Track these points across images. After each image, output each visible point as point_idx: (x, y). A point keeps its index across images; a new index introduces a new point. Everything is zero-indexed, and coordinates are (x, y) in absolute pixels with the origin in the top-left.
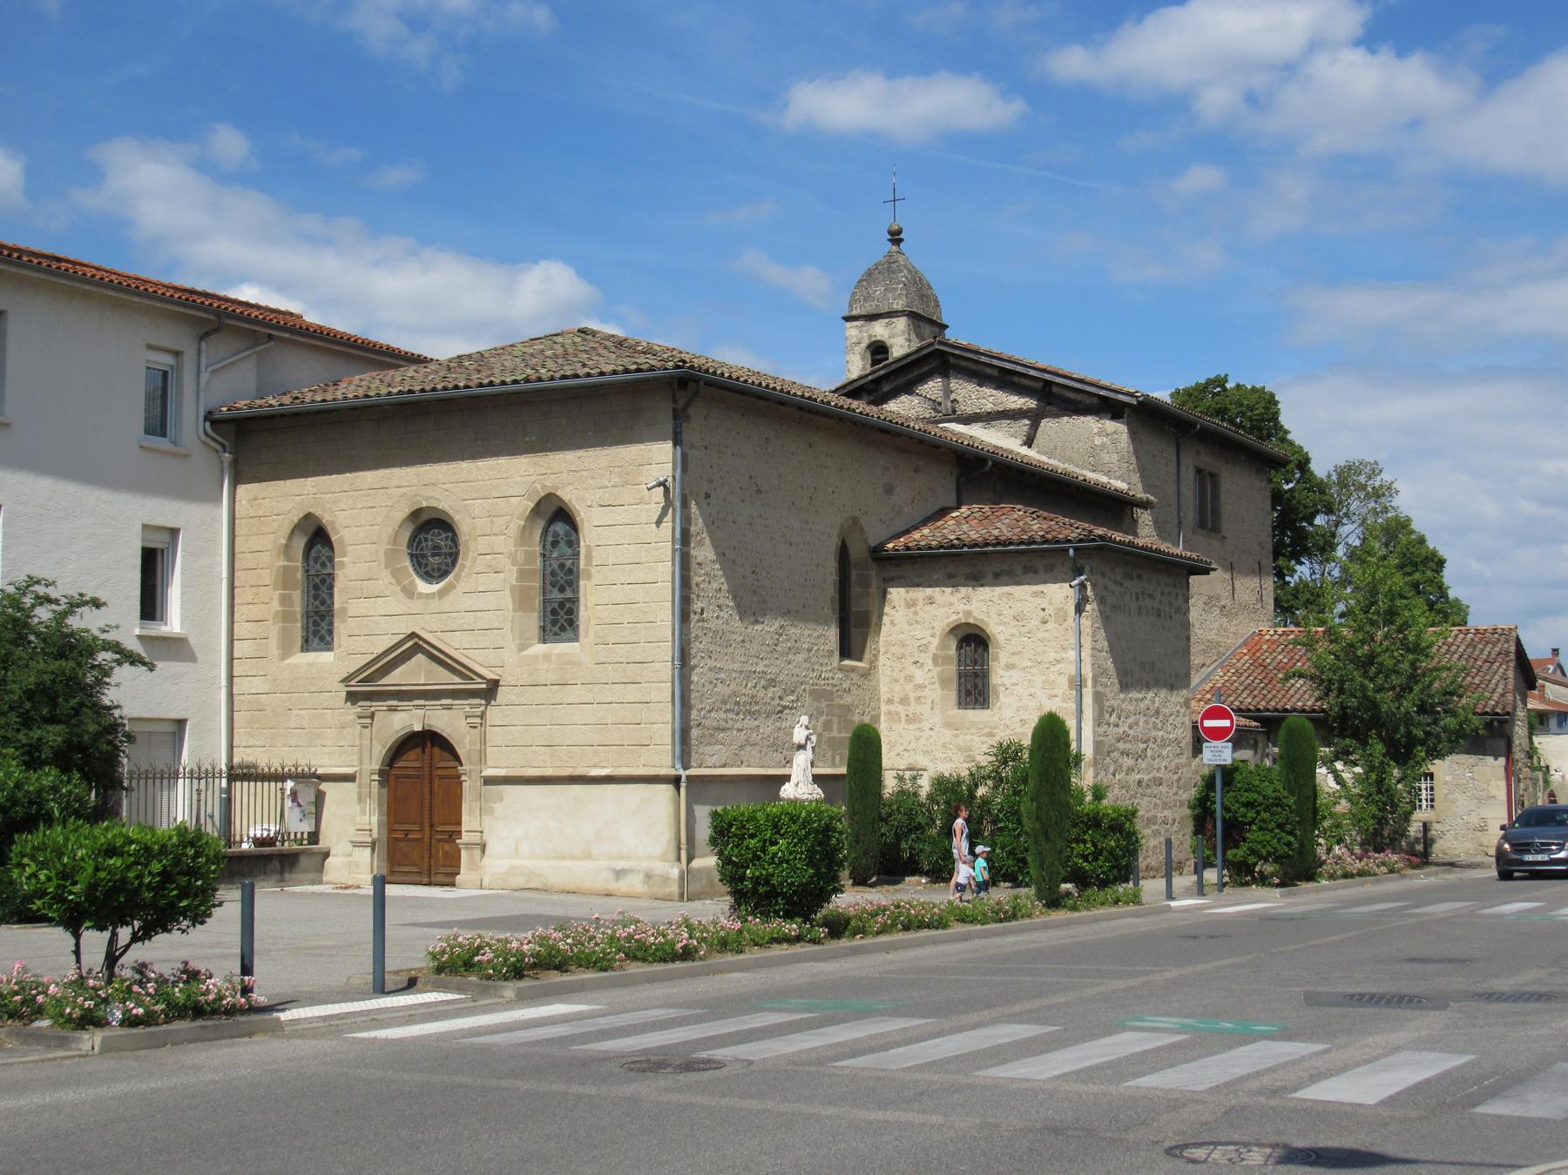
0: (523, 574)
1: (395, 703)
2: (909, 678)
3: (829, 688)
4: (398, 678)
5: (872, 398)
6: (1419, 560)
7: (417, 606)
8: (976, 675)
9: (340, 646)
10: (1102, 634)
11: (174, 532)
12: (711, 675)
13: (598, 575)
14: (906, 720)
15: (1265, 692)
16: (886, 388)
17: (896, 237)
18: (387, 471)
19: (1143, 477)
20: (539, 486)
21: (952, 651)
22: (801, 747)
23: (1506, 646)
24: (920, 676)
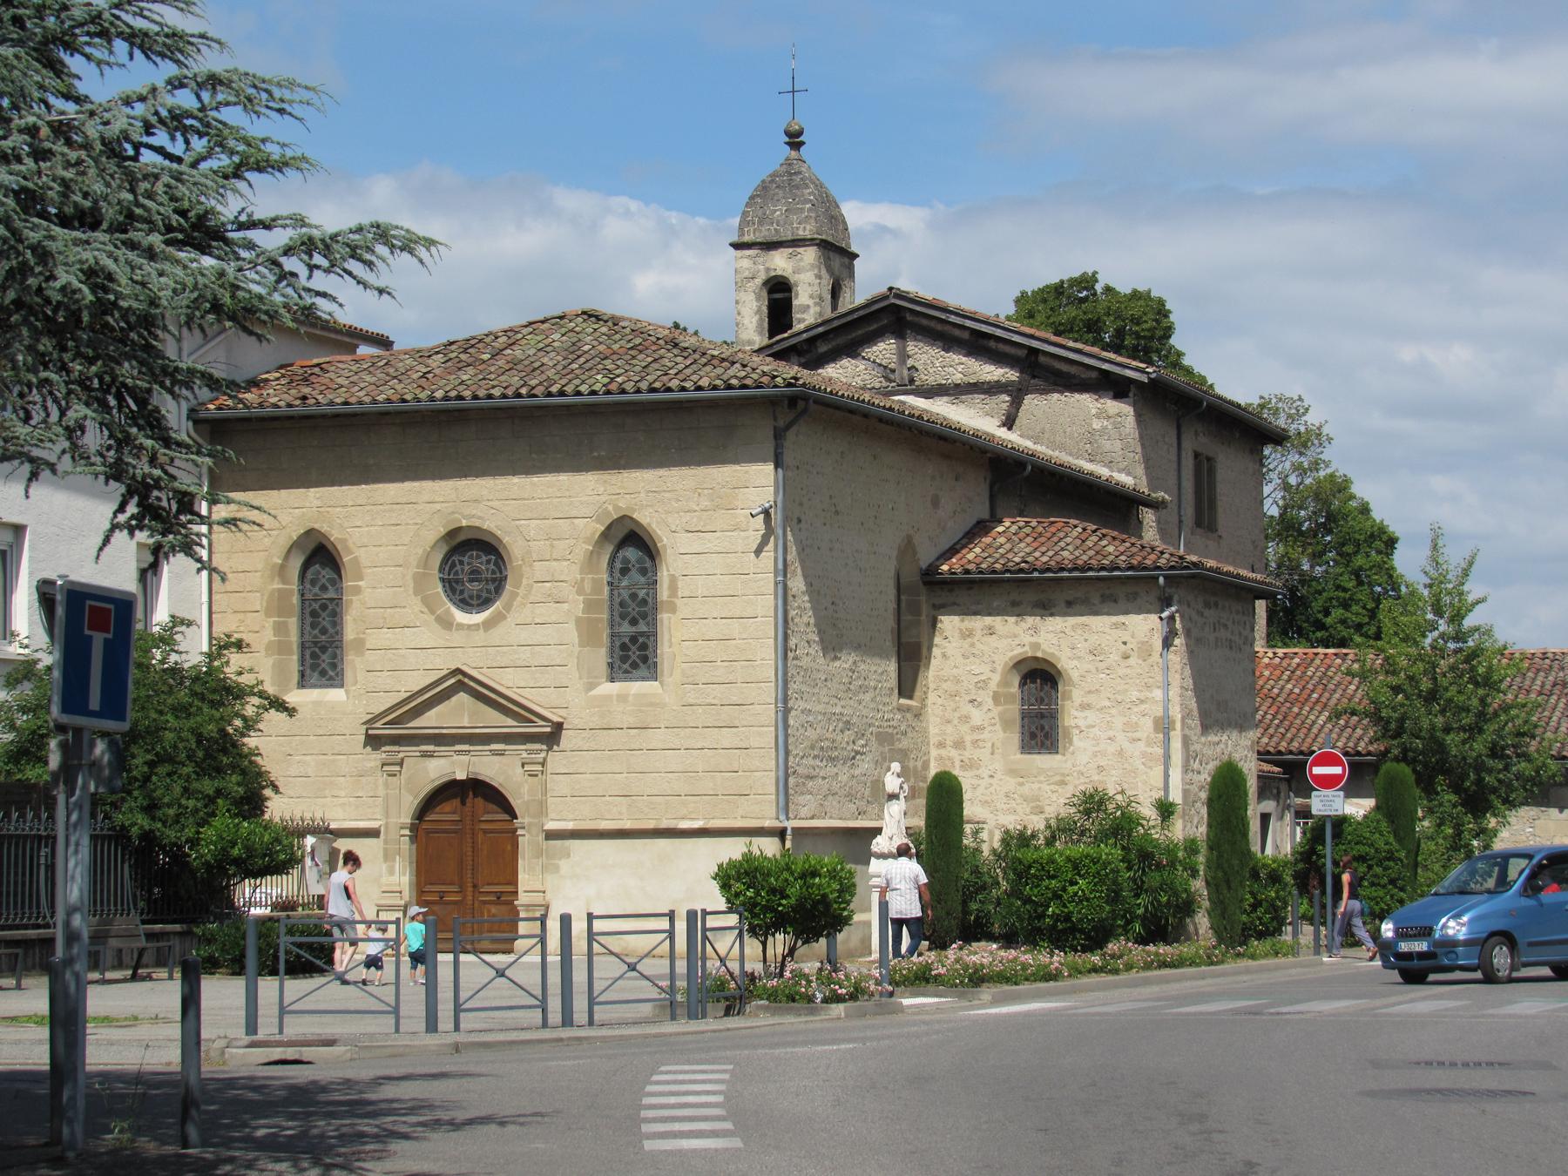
0: (590, 606)
1: (431, 748)
2: (965, 719)
3: (890, 730)
4: (431, 720)
5: (803, 360)
6: (1362, 537)
7: (457, 638)
8: (1042, 716)
9: (356, 683)
10: (1188, 671)
11: (19, 530)
12: (804, 718)
13: (684, 608)
14: (961, 766)
15: (1282, 730)
16: (823, 348)
17: (795, 140)
18: (416, 484)
19: (1147, 468)
20: (610, 508)
21: (1015, 688)
22: (893, 797)
23: (1561, 674)
24: (977, 716)
